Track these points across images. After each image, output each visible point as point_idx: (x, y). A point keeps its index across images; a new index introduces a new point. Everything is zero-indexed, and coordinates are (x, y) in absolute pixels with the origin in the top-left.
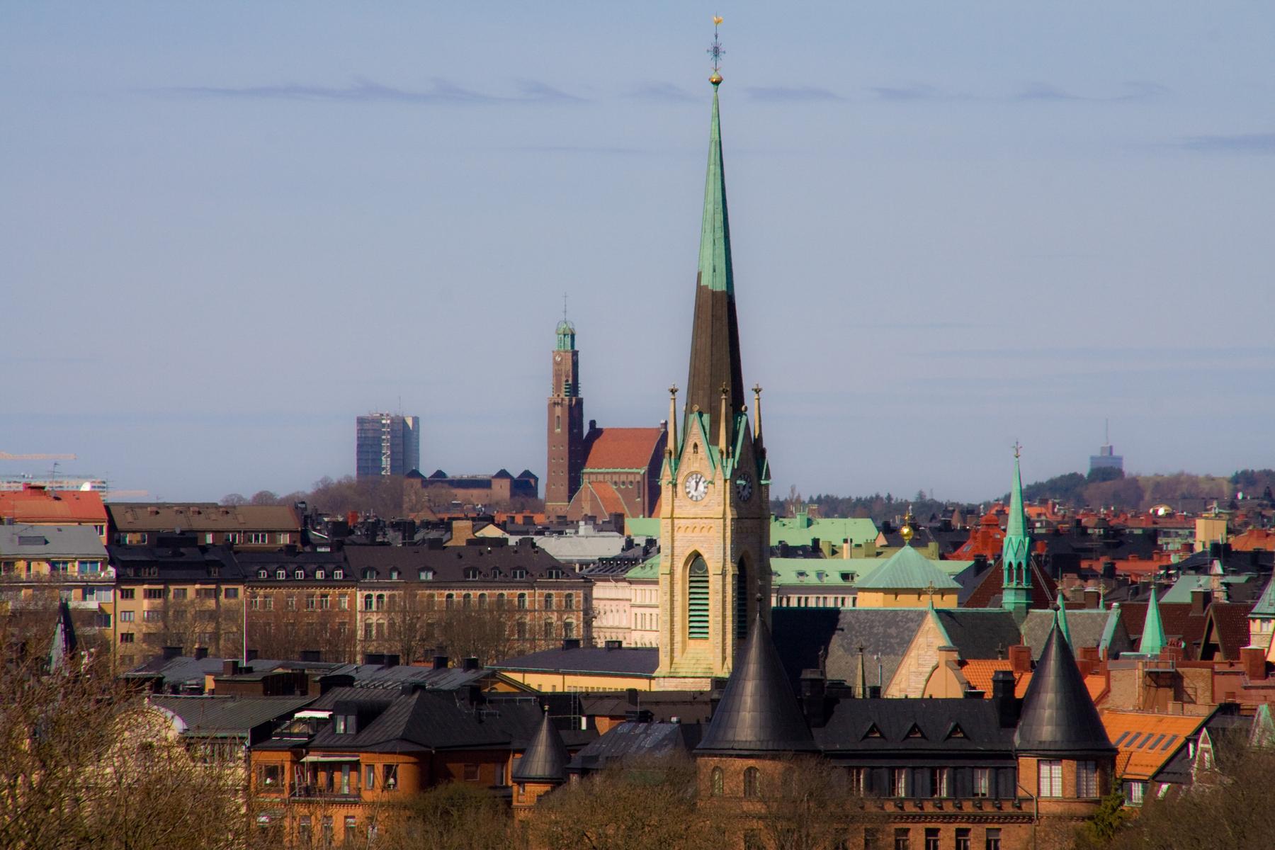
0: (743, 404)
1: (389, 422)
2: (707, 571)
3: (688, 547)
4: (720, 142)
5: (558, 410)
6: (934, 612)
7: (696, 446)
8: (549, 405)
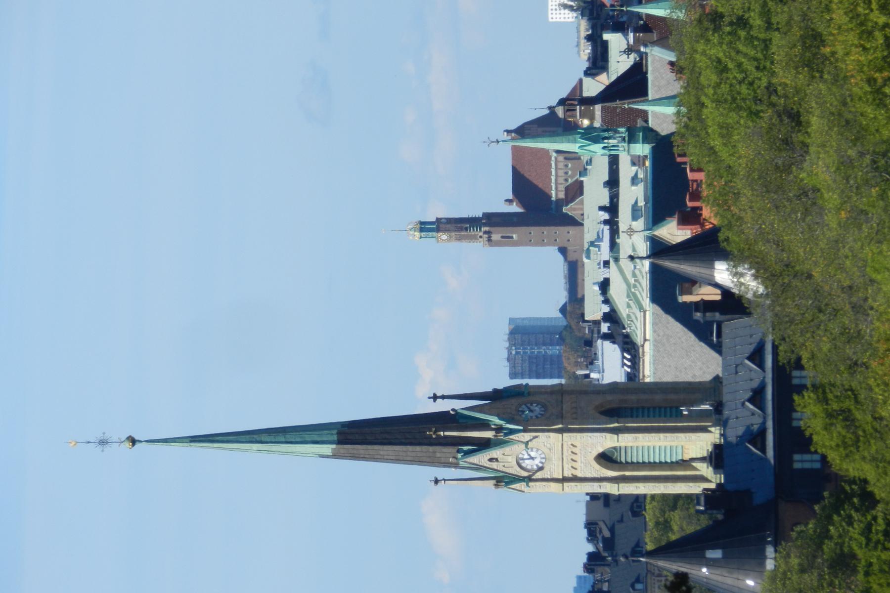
0: (449, 411)
1: (514, 348)
2: (615, 448)
3: (591, 466)
4: (195, 439)
5: (496, 237)
6: (655, 228)
7: (491, 460)
8: (491, 246)
